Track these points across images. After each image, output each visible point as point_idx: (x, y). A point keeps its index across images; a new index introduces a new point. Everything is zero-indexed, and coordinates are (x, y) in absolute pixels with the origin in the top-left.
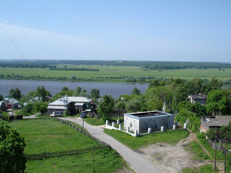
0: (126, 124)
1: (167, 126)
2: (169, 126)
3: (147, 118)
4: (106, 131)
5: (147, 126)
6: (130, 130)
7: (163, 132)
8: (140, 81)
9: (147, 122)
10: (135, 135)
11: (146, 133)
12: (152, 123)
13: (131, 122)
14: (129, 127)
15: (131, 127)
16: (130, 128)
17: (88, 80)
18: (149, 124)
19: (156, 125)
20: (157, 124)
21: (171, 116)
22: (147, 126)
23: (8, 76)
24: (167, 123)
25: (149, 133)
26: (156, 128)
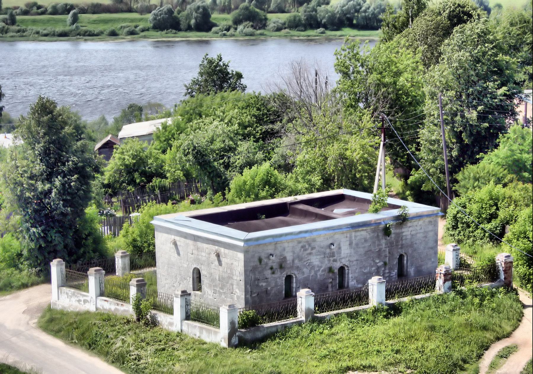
0: (170, 274)
1: (402, 274)
2: (48, 317)
3: (287, 234)
4: (55, 323)
5: (289, 279)
6: (193, 308)
7: (314, 319)
8: (237, 22)
9: (289, 257)
10: (219, 336)
11: (291, 320)
12: (315, 260)
13: (197, 260)
14: (190, 290)
15: (200, 289)
16: (196, 298)
17: (46, 35)
18: (298, 268)
19: (342, 270)
20: (345, 262)
21: (419, 217)
22: (289, 279)
23: (525, 22)
24: (401, 257)
25: (301, 316)
26: (341, 285)
